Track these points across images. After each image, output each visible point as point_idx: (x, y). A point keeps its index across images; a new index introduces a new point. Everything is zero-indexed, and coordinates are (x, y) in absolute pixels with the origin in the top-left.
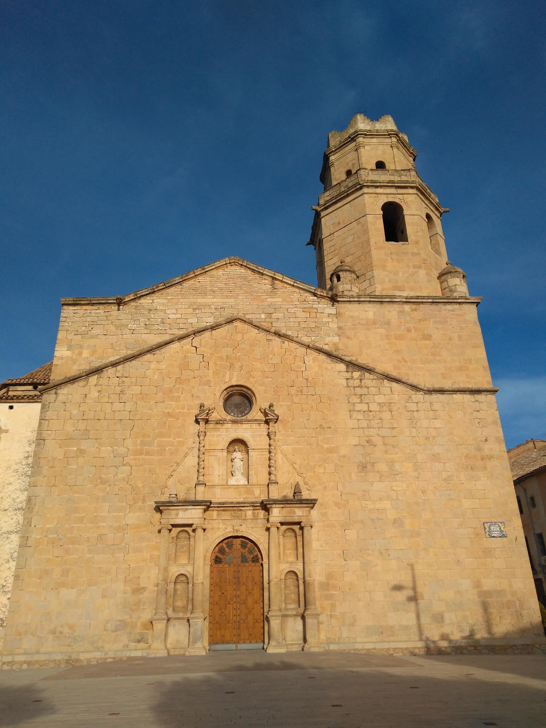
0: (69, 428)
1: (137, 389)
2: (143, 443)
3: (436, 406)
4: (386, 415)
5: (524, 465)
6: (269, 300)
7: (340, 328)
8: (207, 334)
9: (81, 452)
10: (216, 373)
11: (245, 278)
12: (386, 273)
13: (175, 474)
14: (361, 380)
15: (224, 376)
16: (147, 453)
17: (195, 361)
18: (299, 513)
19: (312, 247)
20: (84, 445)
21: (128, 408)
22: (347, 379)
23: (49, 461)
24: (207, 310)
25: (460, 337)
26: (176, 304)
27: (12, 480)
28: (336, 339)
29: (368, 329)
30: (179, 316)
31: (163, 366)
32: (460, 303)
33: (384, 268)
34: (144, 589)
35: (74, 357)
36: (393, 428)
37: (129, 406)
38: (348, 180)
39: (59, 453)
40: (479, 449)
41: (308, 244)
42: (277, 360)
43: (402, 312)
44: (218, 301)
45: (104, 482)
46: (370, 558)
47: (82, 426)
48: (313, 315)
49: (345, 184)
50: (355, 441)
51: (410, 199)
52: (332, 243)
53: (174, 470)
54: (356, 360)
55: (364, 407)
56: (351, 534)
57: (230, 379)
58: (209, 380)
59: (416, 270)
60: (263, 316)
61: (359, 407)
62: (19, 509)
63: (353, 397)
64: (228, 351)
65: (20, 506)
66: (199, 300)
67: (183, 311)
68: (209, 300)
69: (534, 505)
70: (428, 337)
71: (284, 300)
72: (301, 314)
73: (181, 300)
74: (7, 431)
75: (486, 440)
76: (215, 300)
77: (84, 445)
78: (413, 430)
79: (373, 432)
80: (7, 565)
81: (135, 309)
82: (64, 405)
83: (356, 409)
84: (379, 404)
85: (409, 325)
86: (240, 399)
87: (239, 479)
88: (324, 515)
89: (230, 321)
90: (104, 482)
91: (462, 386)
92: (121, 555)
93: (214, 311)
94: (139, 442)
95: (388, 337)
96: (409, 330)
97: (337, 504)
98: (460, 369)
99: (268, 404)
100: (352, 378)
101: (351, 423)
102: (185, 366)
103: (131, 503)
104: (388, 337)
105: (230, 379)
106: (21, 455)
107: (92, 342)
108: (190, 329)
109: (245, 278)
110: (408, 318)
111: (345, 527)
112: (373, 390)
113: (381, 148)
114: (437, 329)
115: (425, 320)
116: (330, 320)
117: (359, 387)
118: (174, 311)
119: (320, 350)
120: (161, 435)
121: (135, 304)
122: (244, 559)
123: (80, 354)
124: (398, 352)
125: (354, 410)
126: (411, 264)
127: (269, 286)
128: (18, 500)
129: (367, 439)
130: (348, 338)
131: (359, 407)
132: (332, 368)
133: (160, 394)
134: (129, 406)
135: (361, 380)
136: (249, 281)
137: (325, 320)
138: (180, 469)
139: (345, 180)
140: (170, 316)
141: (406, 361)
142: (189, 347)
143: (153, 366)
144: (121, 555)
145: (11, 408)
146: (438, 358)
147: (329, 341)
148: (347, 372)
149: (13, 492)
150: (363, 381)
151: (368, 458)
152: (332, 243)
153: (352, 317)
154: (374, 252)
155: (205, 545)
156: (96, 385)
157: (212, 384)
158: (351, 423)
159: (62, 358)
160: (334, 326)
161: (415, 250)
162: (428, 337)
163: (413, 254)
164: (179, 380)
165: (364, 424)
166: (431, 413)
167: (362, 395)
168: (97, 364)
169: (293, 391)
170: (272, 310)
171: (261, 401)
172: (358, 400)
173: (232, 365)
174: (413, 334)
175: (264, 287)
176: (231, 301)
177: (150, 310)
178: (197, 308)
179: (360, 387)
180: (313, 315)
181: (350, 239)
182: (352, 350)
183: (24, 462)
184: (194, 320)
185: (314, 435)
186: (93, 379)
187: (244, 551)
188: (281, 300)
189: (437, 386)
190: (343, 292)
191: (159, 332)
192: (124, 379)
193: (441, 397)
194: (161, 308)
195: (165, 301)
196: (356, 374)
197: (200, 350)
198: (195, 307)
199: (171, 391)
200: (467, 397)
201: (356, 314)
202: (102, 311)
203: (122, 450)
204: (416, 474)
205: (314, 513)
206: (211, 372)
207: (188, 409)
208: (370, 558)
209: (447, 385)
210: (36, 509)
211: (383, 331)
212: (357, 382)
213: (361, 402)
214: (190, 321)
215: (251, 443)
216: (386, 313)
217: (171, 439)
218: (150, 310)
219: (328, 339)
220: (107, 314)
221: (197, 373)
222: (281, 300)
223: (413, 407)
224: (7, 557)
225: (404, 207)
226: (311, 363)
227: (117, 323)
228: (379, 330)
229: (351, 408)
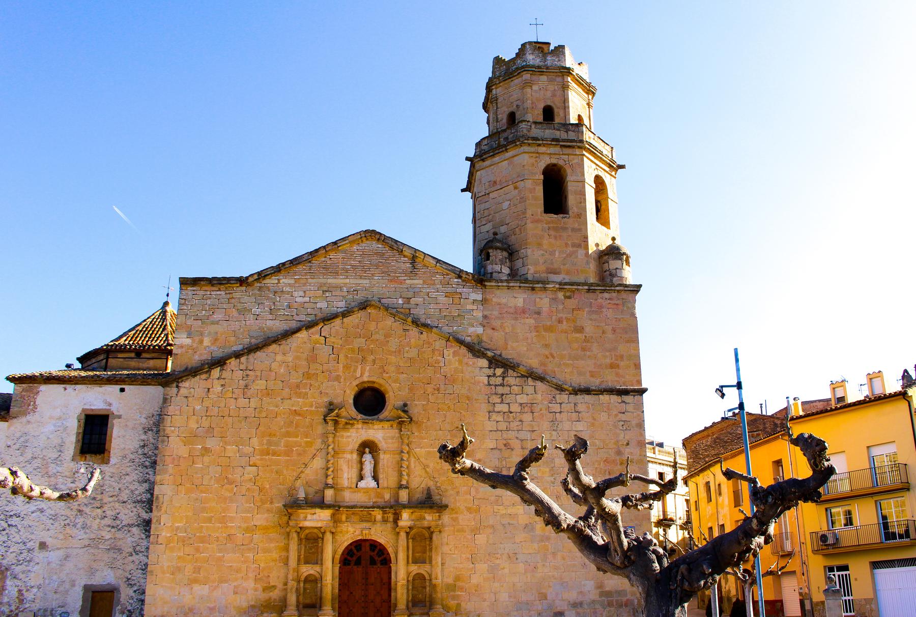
0: (193, 425)
1: (261, 384)
2: (270, 443)
3: (580, 408)
4: (527, 417)
5: (726, 442)
6: (408, 282)
7: (485, 317)
8: (338, 321)
9: (206, 450)
10: (346, 367)
11: (382, 255)
12: (542, 252)
13: (303, 475)
14: (504, 378)
15: (355, 371)
16: (274, 454)
17: (324, 352)
18: (429, 517)
19: (468, 194)
20: (211, 443)
21: (253, 405)
22: (489, 376)
23: (174, 459)
24: (338, 293)
25: (614, 330)
26: (305, 284)
27: (129, 469)
28: (480, 330)
29: (516, 319)
30: (307, 299)
31: (289, 358)
32: (618, 291)
33: (540, 245)
34: (274, 587)
35: (195, 345)
36: (533, 431)
37: (254, 403)
38: (509, 131)
39: (183, 451)
40: (619, 453)
41: (463, 190)
42: (413, 353)
43: (555, 299)
44: (350, 282)
45: (231, 482)
46: (498, 562)
47: (206, 423)
48: (456, 301)
49: (505, 135)
50: (492, 445)
51: (575, 161)
52: (487, 205)
53: (302, 472)
54: (500, 355)
55: (504, 408)
56: (481, 539)
57: (362, 375)
58: (338, 376)
59: (575, 249)
60: (400, 301)
61: (499, 407)
62: (138, 502)
63: (494, 397)
64: (360, 342)
65: (139, 498)
66: (330, 281)
67: (311, 294)
68: (340, 281)
69: (720, 494)
70: (580, 330)
71: (424, 282)
72: (442, 299)
73: (310, 280)
74: (119, 417)
75: (628, 444)
76: (348, 281)
77: (211, 443)
78: (554, 433)
79: (511, 434)
80: (131, 558)
81: (259, 290)
82: (185, 400)
83: (496, 409)
84: (521, 404)
85: (561, 315)
86: (370, 402)
87: (368, 482)
88: (455, 520)
89: (364, 306)
90: (231, 482)
91: (610, 385)
92: (251, 555)
93: (346, 294)
94: (265, 441)
95: (536, 328)
96: (560, 321)
97: (469, 510)
98: (612, 366)
99: (402, 403)
100: (494, 375)
101: (490, 425)
102: (313, 358)
103: (259, 504)
104: (536, 328)
105: (362, 375)
106: (136, 444)
107: (213, 328)
108: (320, 316)
109: (382, 255)
110: (561, 307)
111: (476, 531)
112: (516, 389)
113: (551, 87)
114: (591, 320)
115: (579, 309)
116: (475, 307)
117: (501, 385)
118: (302, 293)
119: (461, 342)
120: (288, 434)
121: (258, 285)
122: (373, 562)
123: (201, 342)
124: (546, 346)
125: (494, 411)
126: (569, 243)
127: (408, 265)
128: (137, 492)
129: (505, 442)
130: (493, 329)
131: (499, 407)
132: (474, 364)
133: (287, 390)
134: (254, 403)
135: (504, 378)
136: (387, 259)
137: (469, 307)
138: (307, 471)
139: (504, 131)
140: (298, 299)
141: (553, 357)
142: (317, 336)
143: (279, 358)
144: (251, 555)
145: (122, 390)
146: (588, 353)
147: (473, 331)
148: (489, 368)
149: (130, 483)
150: (506, 379)
151: (504, 463)
152: (487, 205)
153: (499, 304)
154: (530, 226)
155: (331, 552)
156: (218, 379)
157: (342, 380)
158: (490, 425)
159: (182, 347)
160: (479, 315)
161: (576, 225)
162: (580, 330)
163: (573, 230)
164: (307, 375)
165: (503, 426)
166: (574, 415)
167: (503, 395)
168: (218, 354)
169: (430, 389)
170: (410, 295)
171: (393, 400)
172: (499, 400)
173: (364, 358)
174: (564, 325)
175: (403, 266)
176: (365, 282)
177: (275, 292)
178: (327, 290)
179: (502, 385)
180: (456, 301)
181: (506, 205)
182: (496, 340)
183: (140, 452)
184: (322, 305)
185: (449, 437)
186: (216, 372)
187: (372, 554)
188: (421, 282)
189: (583, 385)
190: (491, 273)
191: (286, 318)
192: (248, 372)
193: (587, 398)
194: (288, 289)
195: (292, 281)
196: (499, 371)
197: (331, 340)
198: (325, 288)
199: (298, 386)
200: (614, 398)
201: (504, 301)
202: (223, 293)
203: (247, 450)
204: (552, 479)
205: (446, 518)
206: (341, 366)
207: (316, 407)
208: (498, 562)
209: (594, 383)
210: (164, 509)
211: (531, 321)
212: (499, 380)
213: (502, 402)
214: (319, 305)
215: (382, 445)
216: (538, 300)
217: (298, 439)
218: (275, 292)
219: (471, 330)
220: (228, 296)
221: (325, 367)
222: (421, 282)
223: (556, 408)
224: (131, 550)
225: (569, 171)
226: (451, 357)
227: (240, 306)
228: (528, 321)
229: (491, 409)
